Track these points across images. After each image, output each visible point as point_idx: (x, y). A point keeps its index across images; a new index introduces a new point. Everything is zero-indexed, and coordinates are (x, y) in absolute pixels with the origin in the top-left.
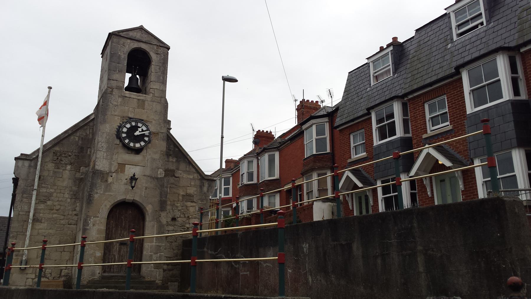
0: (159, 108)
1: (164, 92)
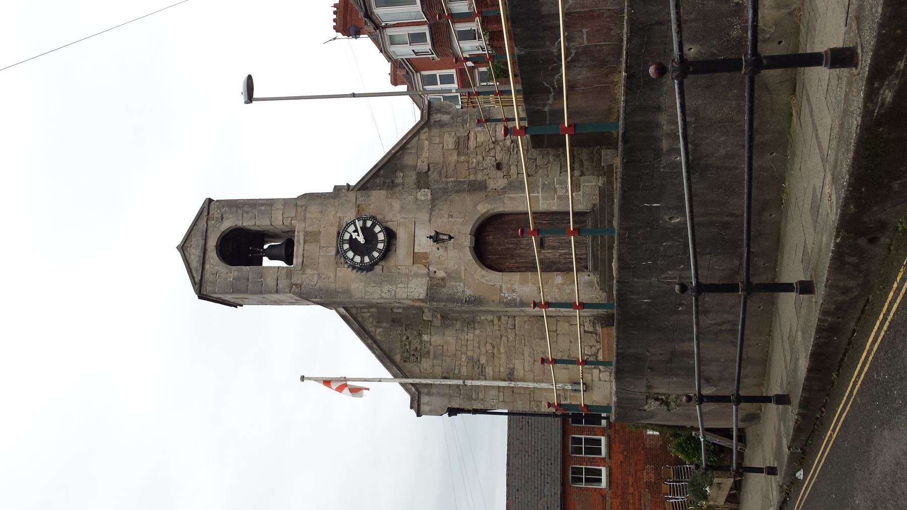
1: (286, 202)
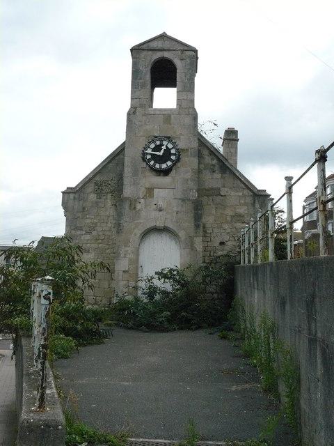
0: (187, 120)
1: (192, 101)
